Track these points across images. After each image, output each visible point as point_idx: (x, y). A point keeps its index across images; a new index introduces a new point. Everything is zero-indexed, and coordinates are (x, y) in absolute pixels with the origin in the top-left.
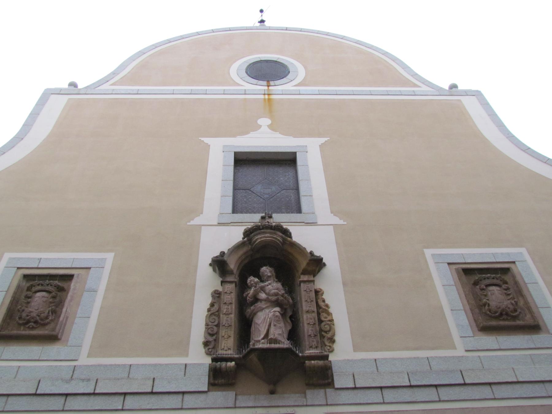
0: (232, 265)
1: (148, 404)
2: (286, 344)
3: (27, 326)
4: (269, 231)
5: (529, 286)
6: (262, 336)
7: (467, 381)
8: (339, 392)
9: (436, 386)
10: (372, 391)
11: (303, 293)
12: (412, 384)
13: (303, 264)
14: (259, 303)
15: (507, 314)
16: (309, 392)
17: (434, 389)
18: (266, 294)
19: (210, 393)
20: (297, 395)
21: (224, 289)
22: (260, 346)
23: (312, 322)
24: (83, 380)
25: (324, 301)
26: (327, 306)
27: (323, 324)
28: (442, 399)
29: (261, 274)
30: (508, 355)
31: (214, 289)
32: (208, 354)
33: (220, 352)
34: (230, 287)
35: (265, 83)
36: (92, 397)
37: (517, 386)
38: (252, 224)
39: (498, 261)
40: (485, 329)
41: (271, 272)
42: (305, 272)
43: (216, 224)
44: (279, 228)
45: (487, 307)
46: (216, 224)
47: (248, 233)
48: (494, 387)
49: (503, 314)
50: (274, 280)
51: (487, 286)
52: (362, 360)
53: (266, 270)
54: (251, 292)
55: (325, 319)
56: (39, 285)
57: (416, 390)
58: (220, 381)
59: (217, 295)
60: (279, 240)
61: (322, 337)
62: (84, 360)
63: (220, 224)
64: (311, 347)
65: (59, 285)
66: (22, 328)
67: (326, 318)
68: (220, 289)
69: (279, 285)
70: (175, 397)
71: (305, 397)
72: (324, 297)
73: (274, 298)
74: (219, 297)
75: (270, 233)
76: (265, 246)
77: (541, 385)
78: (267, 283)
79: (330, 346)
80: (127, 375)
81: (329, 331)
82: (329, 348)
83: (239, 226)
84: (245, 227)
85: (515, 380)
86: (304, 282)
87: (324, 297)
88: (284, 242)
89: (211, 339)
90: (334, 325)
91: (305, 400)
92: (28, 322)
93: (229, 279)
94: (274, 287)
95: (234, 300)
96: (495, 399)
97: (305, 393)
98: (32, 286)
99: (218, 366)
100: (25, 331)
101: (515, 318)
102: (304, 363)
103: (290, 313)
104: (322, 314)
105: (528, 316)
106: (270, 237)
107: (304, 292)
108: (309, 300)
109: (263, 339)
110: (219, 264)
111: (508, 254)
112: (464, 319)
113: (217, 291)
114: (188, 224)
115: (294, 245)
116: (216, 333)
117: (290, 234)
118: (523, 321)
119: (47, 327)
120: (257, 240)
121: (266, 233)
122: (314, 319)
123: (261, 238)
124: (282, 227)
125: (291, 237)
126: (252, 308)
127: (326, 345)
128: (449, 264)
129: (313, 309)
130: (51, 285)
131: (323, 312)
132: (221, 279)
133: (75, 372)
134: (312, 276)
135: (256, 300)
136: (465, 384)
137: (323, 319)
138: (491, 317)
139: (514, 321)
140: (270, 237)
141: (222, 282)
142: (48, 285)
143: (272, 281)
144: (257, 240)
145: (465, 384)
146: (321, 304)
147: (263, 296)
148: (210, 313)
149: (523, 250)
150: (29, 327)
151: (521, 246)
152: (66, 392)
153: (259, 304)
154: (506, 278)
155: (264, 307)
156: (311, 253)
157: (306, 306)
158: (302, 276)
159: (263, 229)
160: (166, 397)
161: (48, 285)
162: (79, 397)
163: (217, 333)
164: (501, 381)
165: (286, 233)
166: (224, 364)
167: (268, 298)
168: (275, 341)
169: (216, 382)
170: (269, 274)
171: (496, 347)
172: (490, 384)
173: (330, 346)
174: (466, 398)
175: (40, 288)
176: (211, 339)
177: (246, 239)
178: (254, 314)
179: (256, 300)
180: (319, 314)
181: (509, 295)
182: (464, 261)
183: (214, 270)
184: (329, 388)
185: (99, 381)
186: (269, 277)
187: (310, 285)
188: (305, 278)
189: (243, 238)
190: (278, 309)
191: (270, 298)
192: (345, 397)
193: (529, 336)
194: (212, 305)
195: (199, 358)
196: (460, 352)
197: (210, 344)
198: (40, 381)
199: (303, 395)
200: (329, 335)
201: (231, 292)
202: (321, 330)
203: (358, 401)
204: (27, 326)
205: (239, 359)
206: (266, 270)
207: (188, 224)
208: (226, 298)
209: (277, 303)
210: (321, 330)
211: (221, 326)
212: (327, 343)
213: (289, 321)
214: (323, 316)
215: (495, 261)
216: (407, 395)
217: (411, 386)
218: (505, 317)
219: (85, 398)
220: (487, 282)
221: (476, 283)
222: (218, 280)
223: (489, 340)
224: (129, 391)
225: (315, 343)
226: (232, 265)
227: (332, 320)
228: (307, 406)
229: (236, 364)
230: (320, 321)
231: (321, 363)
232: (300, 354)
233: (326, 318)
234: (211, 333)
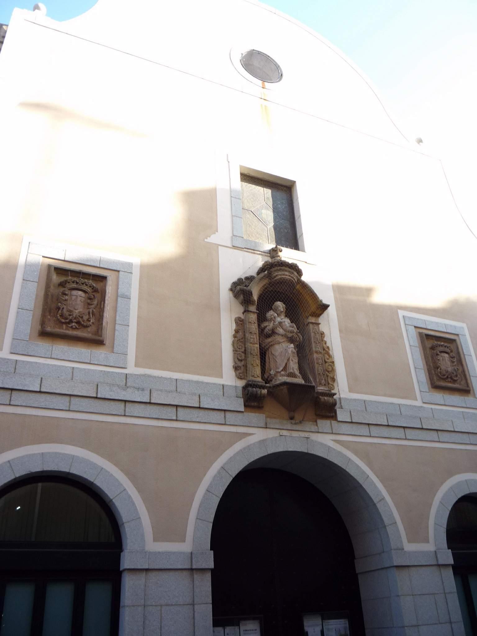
1: (197, 417)
3: (70, 326)
4: (287, 269)
5: (466, 357)
6: (281, 369)
7: (424, 427)
8: (341, 424)
9: (404, 427)
10: (363, 426)
12: (390, 424)
14: (277, 337)
15: (451, 378)
16: (319, 421)
17: (402, 430)
19: (245, 414)
20: (311, 423)
24: (138, 389)
28: (408, 437)
30: (448, 409)
31: (237, 316)
32: (240, 378)
34: (253, 317)
35: (260, 82)
36: (148, 405)
37: (453, 434)
39: (448, 331)
40: (435, 387)
45: (439, 369)
48: (440, 433)
49: (450, 377)
51: (441, 352)
52: (355, 400)
53: (280, 305)
56: (73, 282)
57: (391, 429)
58: (252, 404)
59: (240, 322)
62: (132, 369)
64: (320, 384)
65: (93, 286)
66: (64, 326)
68: (243, 317)
70: (219, 413)
71: (317, 425)
73: (290, 335)
75: (289, 272)
77: (467, 435)
80: (175, 389)
81: (331, 371)
83: (252, 253)
85: (453, 430)
86: (312, 323)
89: (240, 364)
91: (316, 427)
92: (71, 321)
96: (439, 442)
97: (316, 422)
98: (66, 282)
100: (69, 330)
101: (454, 381)
105: (463, 382)
110: (240, 290)
111: (455, 327)
112: (423, 377)
113: (240, 318)
114: (206, 240)
115: (305, 286)
118: (460, 385)
119: (89, 329)
121: (286, 271)
123: (281, 275)
128: (415, 327)
130: (86, 285)
133: (128, 380)
135: (273, 332)
136: (422, 429)
138: (440, 378)
139: (454, 383)
140: (290, 276)
142: (83, 284)
145: (422, 429)
147: (280, 331)
148: (236, 339)
149: (464, 325)
150: (72, 327)
151: (463, 322)
152: (125, 399)
154: (452, 346)
158: (310, 317)
160: (211, 413)
161: (83, 284)
162: (136, 404)
163: (245, 359)
164: (444, 429)
167: (286, 334)
170: (282, 310)
171: (442, 403)
172: (437, 430)
174: (422, 439)
175: (74, 285)
176: (240, 364)
181: (453, 362)
182: (425, 327)
185: (152, 392)
186: (282, 312)
191: (287, 333)
192: (345, 428)
193: (463, 397)
194: (237, 331)
195: (229, 378)
196: (418, 403)
197: (240, 368)
198: (98, 385)
199: (315, 423)
203: (353, 433)
204: (70, 326)
207: (206, 240)
209: (291, 340)
212: (330, 382)
215: (445, 331)
216: (385, 432)
217: (388, 426)
218: (449, 380)
219: (143, 406)
220: (441, 349)
221: (432, 348)
222: (242, 309)
223: (439, 396)
224: (180, 404)
227: (333, 362)
228: (318, 432)
232: (70, 278)
233: (328, 359)
234: (240, 358)
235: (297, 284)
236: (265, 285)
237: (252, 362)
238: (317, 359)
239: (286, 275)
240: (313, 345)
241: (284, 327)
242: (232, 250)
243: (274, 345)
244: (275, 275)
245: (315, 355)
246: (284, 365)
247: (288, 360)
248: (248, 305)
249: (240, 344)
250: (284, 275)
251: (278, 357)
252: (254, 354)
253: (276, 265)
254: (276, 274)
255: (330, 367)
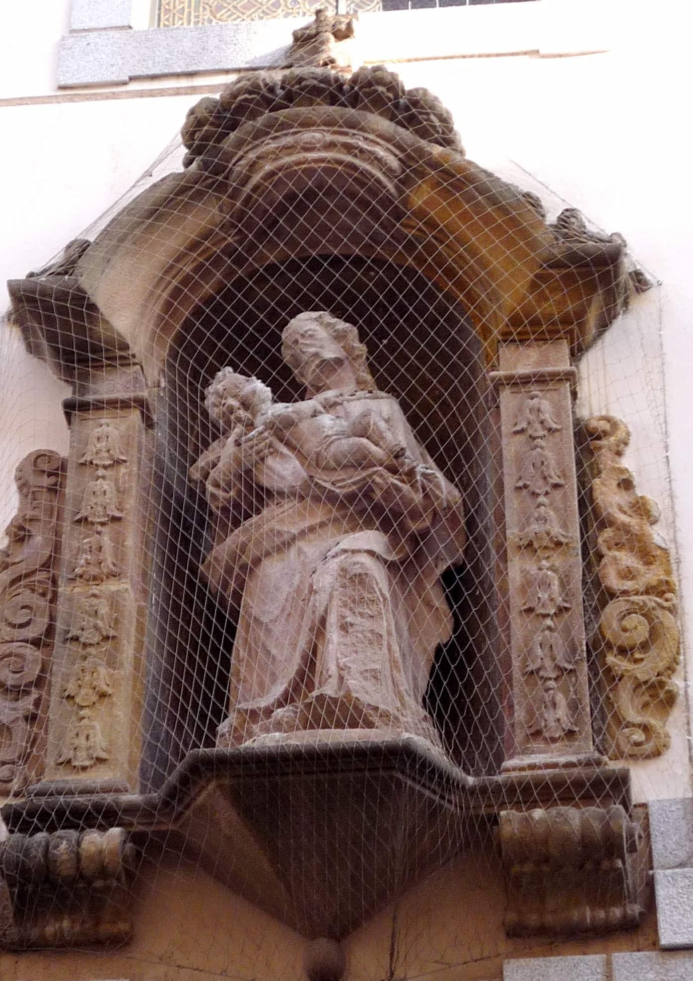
0: (126, 306)
2: (420, 735)
6: (278, 690)
11: (511, 447)
13: (508, 286)
18: (302, 457)
21: (80, 443)
22: (266, 740)
23: (551, 595)
25: (626, 484)
26: (641, 508)
27: (613, 609)
29: (287, 356)
33: (54, 778)
38: (232, 78)
41: (339, 337)
42: (526, 330)
43: (47, 89)
44: (374, 93)
46: (47, 89)
47: (213, 131)
50: (360, 383)
53: (315, 333)
54: (224, 454)
55: (628, 585)
60: (378, 161)
61: (604, 680)
63: (69, 90)
67: (628, 574)
69: (384, 411)
72: (626, 462)
73: (344, 483)
74: (53, 490)
75: (329, 123)
76: (307, 196)
78: (305, 406)
79: (646, 728)
82: (639, 736)
84: (193, 100)
87: (626, 462)
88: (414, 166)
90: (673, 610)
93: (110, 385)
94: (355, 414)
95: (131, 503)
99: (38, 853)
102: (495, 820)
103: (444, 556)
104: (610, 554)
106: (331, 146)
107: (521, 433)
108: (539, 487)
109: (285, 699)
115: (463, 184)
116: (39, 682)
117: (445, 120)
120: (253, 166)
121: (307, 124)
122: (564, 584)
123: (276, 155)
124: (393, 86)
125: (447, 140)
126: (234, 539)
127: (619, 720)
129: (556, 530)
131: (619, 546)
132: (67, 393)
134: (565, 348)
135: (539, 559)
137: (613, 581)
141: (70, 408)
143: (352, 386)
144: (253, 166)
146: (610, 498)
147: (284, 470)
153: (277, 519)
155: (295, 531)
156: (568, 218)
157: (532, 518)
158: (507, 353)
159: (290, 97)
165: (415, 114)
166: (63, 842)
168: (349, 712)
169: (34, 933)
170: (331, 352)
173: (646, 728)
177: (194, 165)
178: (245, 569)
179: (254, 495)
180: (591, 556)
183: (33, 349)
184: (620, 951)
186: (330, 367)
187: (545, 403)
188: (521, 361)
189: (188, 163)
190: (372, 539)
191: (325, 481)
200: (644, 671)
201: (118, 462)
202: (597, 647)
205: (146, 812)
206: (315, 333)
208: (101, 492)
209: (365, 507)
210: (597, 647)
211: (57, 639)
212: (632, 715)
213: (439, 602)
214: (618, 562)
225: (562, 712)
226: (126, 306)
227: (663, 589)
229: (137, 838)
230: (599, 595)
231: (574, 818)
235: (405, 182)
236: (207, 235)
237: (71, 688)
238: (528, 584)
239: (378, 145)
240: (513, 505)
241: (312, 446)
242: (68, 108)
243: (257, 561)
244: (240, 168)
245: (517, 569)
246: (296, 662)
247: (320, 628)
248: (84, 376)
249: (26, 597)
250: (289, 149)
251: (277, 629)
252: (87, 636)
253: (241, 109)
254: (252, 156)
255: (635, 619)
